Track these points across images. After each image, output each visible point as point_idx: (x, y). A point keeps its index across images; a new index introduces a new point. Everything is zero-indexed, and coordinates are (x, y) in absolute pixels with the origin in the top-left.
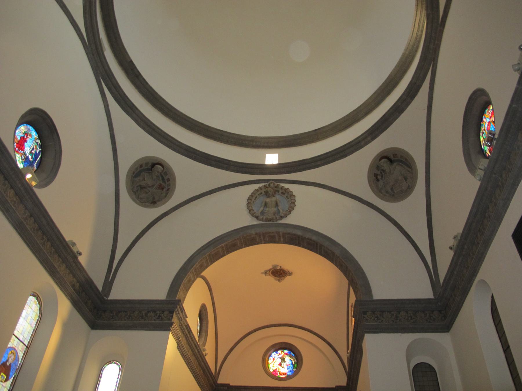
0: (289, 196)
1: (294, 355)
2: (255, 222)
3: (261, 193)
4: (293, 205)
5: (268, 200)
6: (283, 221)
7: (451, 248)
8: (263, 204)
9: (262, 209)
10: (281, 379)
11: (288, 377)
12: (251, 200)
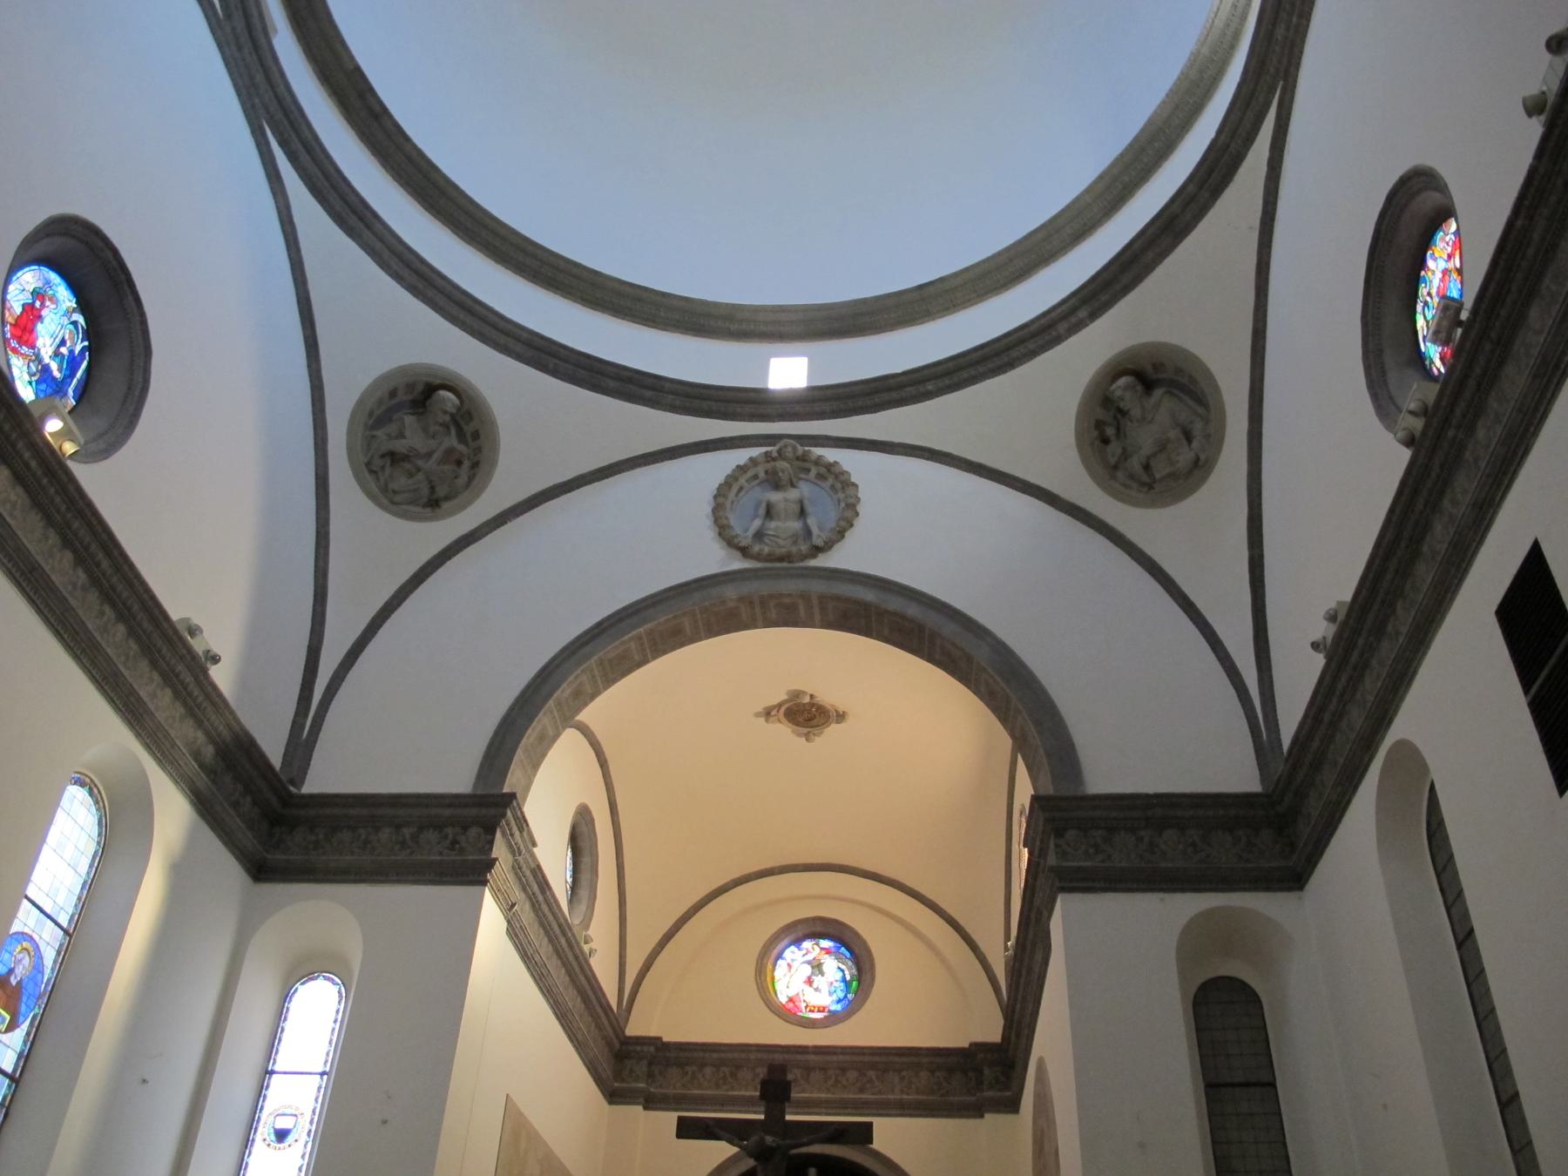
0: (839, 486)
1: (848, 954)
2: (738, 564)
3: (756, 477)
4: (849, 514)
5: (775, 497)
6: (822, 561)
7: (1315, 646)
8: (762, 511)
9: (757, 523)
10: (812, 1024)
11: (833, 1019)
12: (725, 496)
